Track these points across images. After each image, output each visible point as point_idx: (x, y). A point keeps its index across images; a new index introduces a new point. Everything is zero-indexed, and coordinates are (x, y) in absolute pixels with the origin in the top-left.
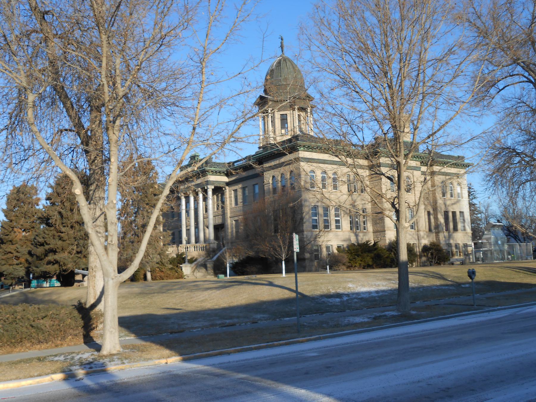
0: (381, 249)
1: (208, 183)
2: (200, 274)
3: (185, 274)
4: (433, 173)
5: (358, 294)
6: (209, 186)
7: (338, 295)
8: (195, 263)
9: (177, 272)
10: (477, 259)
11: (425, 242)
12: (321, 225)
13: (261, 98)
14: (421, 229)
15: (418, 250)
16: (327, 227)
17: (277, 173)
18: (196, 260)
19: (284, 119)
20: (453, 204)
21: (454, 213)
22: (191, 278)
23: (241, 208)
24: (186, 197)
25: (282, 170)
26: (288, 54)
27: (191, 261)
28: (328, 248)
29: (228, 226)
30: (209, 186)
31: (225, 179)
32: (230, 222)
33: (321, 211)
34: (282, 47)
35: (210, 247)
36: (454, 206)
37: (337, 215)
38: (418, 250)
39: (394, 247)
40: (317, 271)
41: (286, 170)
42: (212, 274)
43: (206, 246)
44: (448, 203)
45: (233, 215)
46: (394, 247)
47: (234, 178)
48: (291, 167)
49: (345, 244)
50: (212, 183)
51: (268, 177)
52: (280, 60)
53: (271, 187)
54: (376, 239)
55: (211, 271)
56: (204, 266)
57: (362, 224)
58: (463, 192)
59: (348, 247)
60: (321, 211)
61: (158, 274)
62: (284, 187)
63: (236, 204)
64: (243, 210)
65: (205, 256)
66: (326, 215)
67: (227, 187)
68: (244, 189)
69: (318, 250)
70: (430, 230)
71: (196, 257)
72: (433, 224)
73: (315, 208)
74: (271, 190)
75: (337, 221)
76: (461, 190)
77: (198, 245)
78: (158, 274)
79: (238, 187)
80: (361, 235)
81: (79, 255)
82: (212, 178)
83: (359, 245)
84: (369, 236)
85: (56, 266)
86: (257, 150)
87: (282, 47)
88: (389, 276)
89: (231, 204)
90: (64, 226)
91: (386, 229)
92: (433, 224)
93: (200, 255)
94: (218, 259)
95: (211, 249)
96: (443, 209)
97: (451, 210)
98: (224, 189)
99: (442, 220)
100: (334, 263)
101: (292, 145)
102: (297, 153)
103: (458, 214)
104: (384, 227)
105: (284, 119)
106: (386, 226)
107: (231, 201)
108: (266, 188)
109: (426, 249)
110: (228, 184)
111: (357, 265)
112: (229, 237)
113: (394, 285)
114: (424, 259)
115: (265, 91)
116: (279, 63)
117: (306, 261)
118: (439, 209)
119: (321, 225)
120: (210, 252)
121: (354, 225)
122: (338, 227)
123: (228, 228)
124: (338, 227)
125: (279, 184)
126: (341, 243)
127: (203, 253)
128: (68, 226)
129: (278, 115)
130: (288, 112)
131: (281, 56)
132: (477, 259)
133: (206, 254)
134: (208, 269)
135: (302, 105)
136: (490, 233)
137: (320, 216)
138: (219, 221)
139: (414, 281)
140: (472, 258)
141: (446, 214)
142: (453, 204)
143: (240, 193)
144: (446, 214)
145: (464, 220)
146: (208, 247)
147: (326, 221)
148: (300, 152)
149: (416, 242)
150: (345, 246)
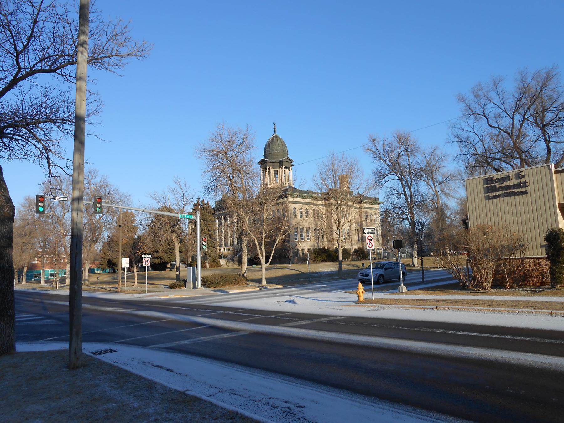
0: (331, 251)
4: (360, 208)
5: (324, 272)
7: (316, 273)
10: (384, 257)
11: (355, 247)
12: (299, 237)
13: (262, 160)
15: (351, 251)
16: (302, 239)
19: (276, 173)
22: (226, 267)
26: (277, 134)
27: (225, 257)
28: (303, 250)
33: (299, 230)
34: (275, 129)
37: (308, 232)
38: (351, 251)
39: (337, 251)
40: (297, 263)
41: (281, 207)
46: (337, 251)
49: (312, 248)
56: (233, 260)
59: (313, 250)
60: (299, 230)
66: (302, 232)
69: (298, 251)
70: (359, 240)
72: (360, 237)
75: (308, 236)
77: (227, 248)
83: (320, 249)
84: (324, 244)
85: (159, 260)
87: (275, 129)
88: (336, 266)
92: (360, 237)
100: (303, 259)
105: (276, 173)
109: (356, 251)
113: (337, 269)
114: (354, 256)
115: (265, 156)
116: (273, 139)
119: (299, 237)
121: (317, 238)
122: (308, 239)
124: (308, 239)
126: (309, 248)
127: (230, 252)
129: (272, 170)
130: (278, 169)
132: (384, 257)
139: (344, 267)
140: (382, 256)
147: (302, 236)
149: (350, 247)
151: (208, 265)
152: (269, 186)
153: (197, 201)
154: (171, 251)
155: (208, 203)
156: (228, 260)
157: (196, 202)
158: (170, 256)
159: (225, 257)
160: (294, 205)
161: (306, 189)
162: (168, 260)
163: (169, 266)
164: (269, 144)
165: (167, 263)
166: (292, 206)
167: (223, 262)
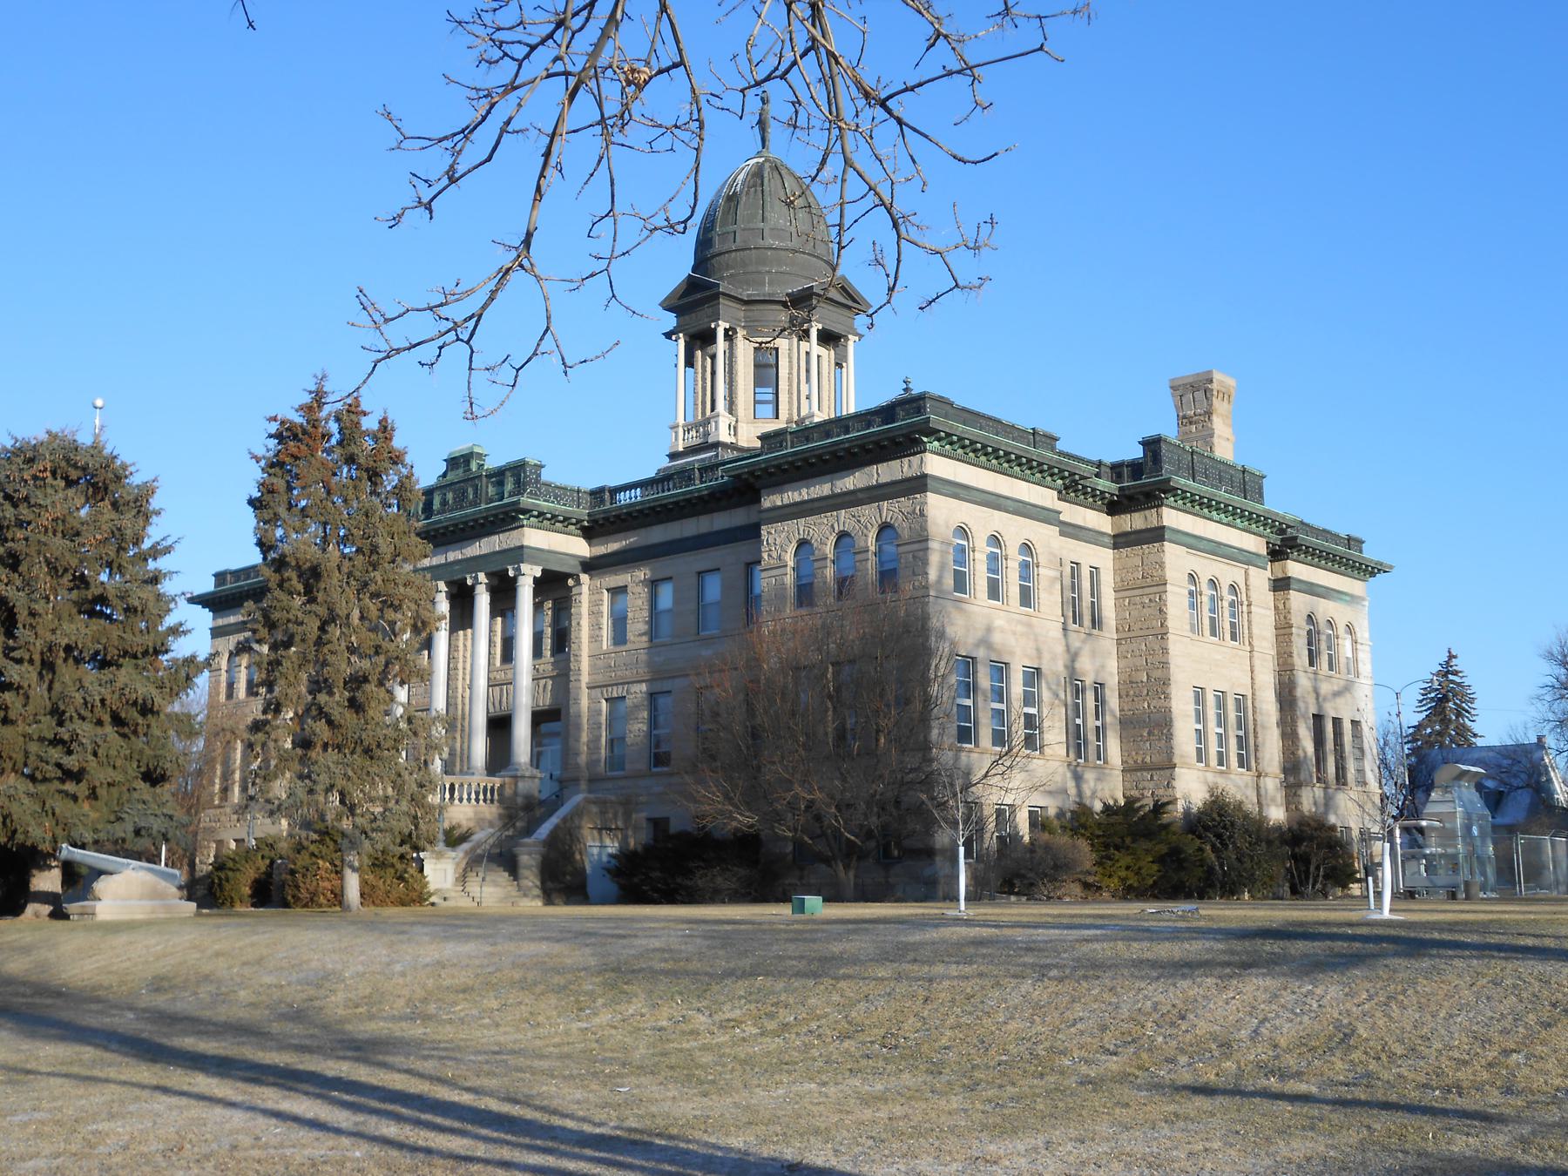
1: (518, 554)
2: (491, 892)
3: (432, 887)
6: (525, 568)
8: (466, 846)
9: (401, 878)
14: (1269, 770)
17: (822, 531)
18: (464, 838)
19: (766, 371)
20: (1337, 694)
21: (1337, 722)
23: (643, 656)
24: (494, 591)
25: (844, 519)
27: (454, 839)
29: (579, 716)
30: (525, 568)
31: (579, 547)
32: (586, 702)
35: (516, 793)
36: (1340, 701)
41: (865, 522)
42: (537, 892)
43: (502, 786)
44: (1325, 688)
45: (600, 679)
47: (613, 546)
48: (890, 510)
50: (537, 555)
51: (779, 545)
52: (760, 167)
53: (789, 579)
54: (1135, 793)
55: (531, 879)
56: (505, 860)
57: (1092, 737)
58: (1361, 656)
59: (1061, 814)
60: (984, 681)
61: (327, 884)
62: (843, 583)
63: (620, 636)
64: (650, 664)
65: (499, 824)
67: (584, 578)
68: (653, 584)
71: (465, 825)
73: (969, 663)
74: (791, 591)
76: (1355, 650)
78: (327, 884)
79: (635, 578)
80: (1090, 776)
81: (70, 787)
82: (534, 537)
86: (665, 463)
89: (595, 638)
90: (19, 661)
91: (1176, 760)
93: (480, 821)
94: (553, 841)
95: (520, 800)
96: (1313, 710)
97: (1330, 712)
98: (571, 582)
99: (1307, 744)
101: (899, 428)
102: (915, 460)
103: (1347, 727)
104: (1170, 752)
105: (766, 371)
106: (1177, 751)
107: (596, 626)
108: (764, 582)
110: (590, 566)
111: (1114, 883)
112: (583, 759)
116: (758, 173)
117: (938, 859)
118: (1301, 704)
120: (521, 814)
123: (578, 727)
125: (829, 572)
126: (1039, 800)
127: (490, 811)
128: (31, 661)
129: (745, 351)
131: (759, 154)
133: (501, 816)
134: (524, 872)
135: (836, 323)
136: (1448, 797)
137: (980, 699)
138: (546, 701)
141: (1318, 718)
142: (1337, 694)
143: (637, 603)
144: (1318, 718)
145: (1362, 750)
146: (508, 791)
148: (928, 456)
150: (1052, 812)
151: (353, 884)
152: (724, 436)
153: (307, 409)
154: (71, 762)
155: (385, 429)
156: (474, 862)
157: (298, 419)
158: (60, 806)
159: (454, 839)
160: (964, 509)
161: (1026, 423)
162: (38, 832)
163: (48, 881)
164: (732, 199)
165: (34, 858)
166: (941, 512)
167: (440, 871)
